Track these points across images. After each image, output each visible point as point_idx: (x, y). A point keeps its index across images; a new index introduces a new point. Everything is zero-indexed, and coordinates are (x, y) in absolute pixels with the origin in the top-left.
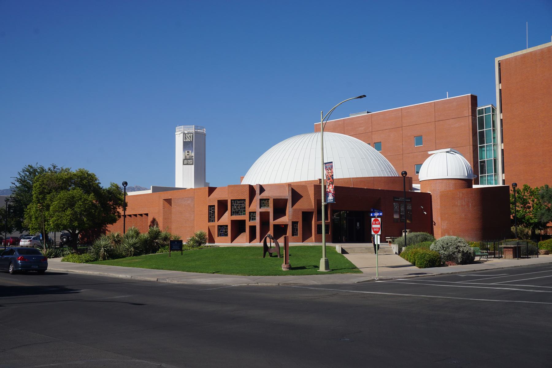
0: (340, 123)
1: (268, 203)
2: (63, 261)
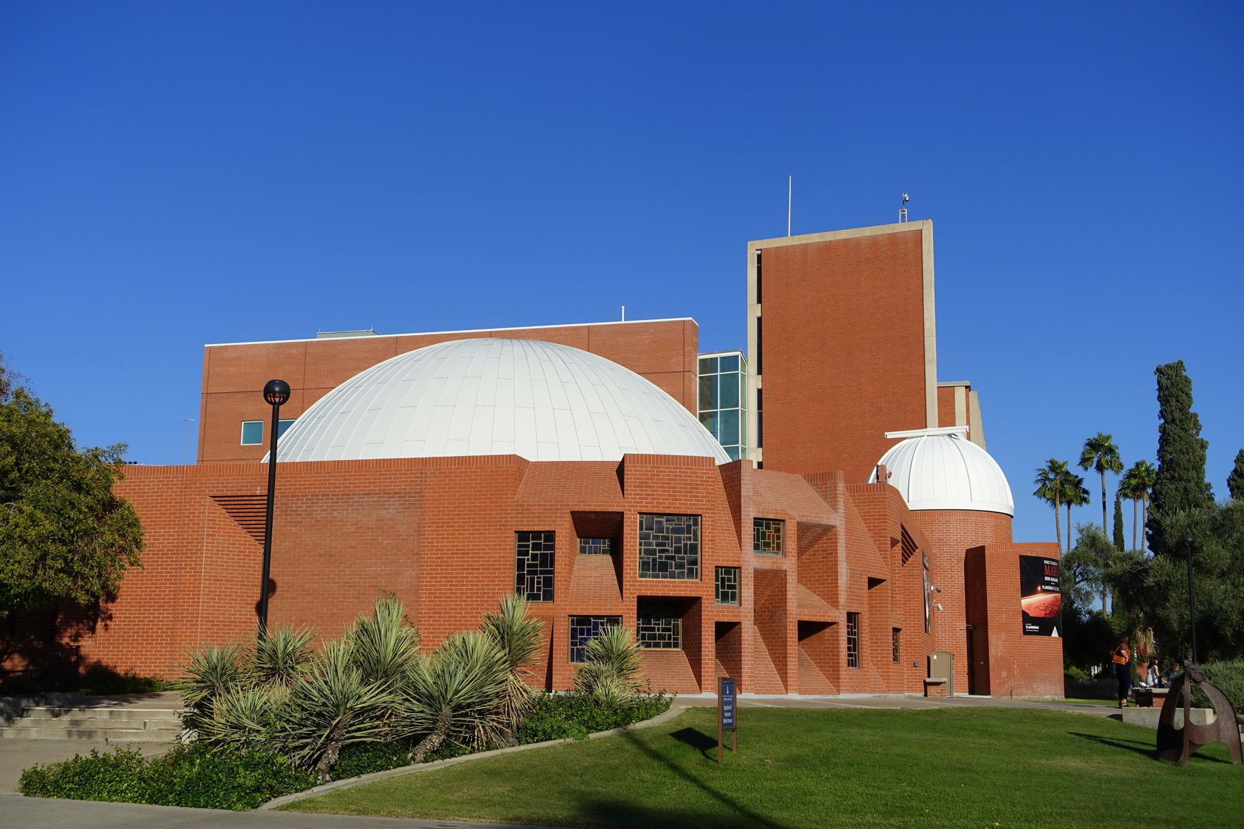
0: (294, 351)
1: (778, 537)
2: (704, 760)
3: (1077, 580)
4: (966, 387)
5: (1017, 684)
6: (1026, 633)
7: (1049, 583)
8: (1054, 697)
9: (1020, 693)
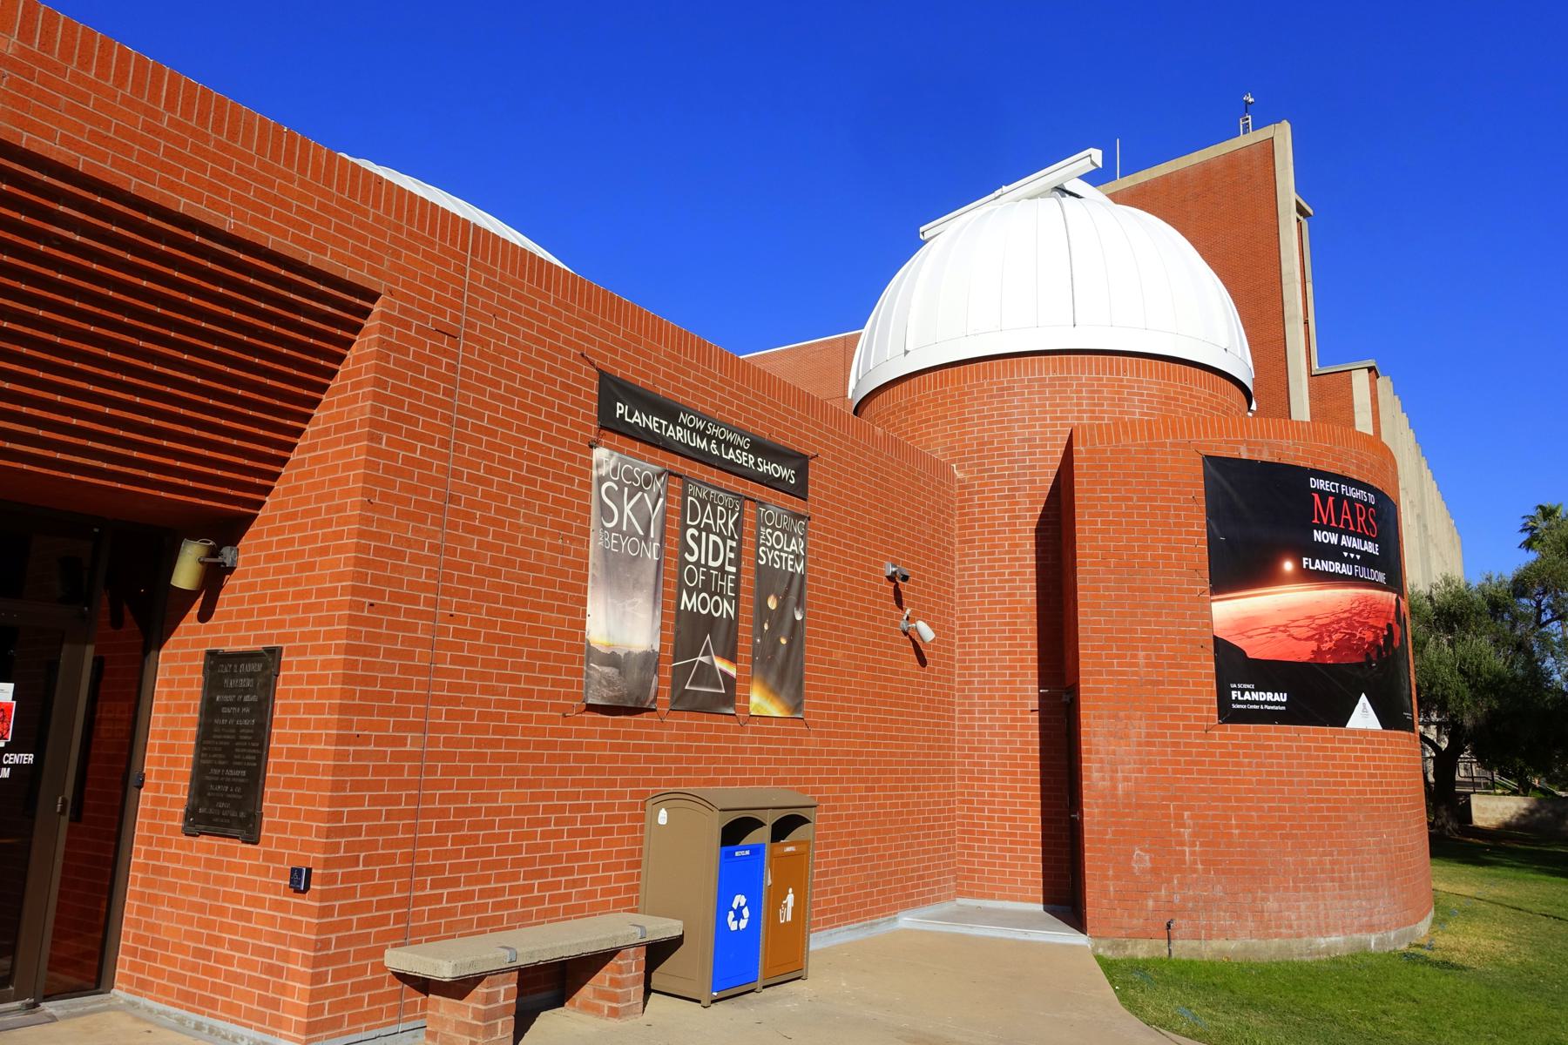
3: (1544, 618)
4: (1370, 369)
5: (1195, 899)
6: (1229, 714)
7: (1334, 553)
8: (1364, 936)
9: (1209, 928)
